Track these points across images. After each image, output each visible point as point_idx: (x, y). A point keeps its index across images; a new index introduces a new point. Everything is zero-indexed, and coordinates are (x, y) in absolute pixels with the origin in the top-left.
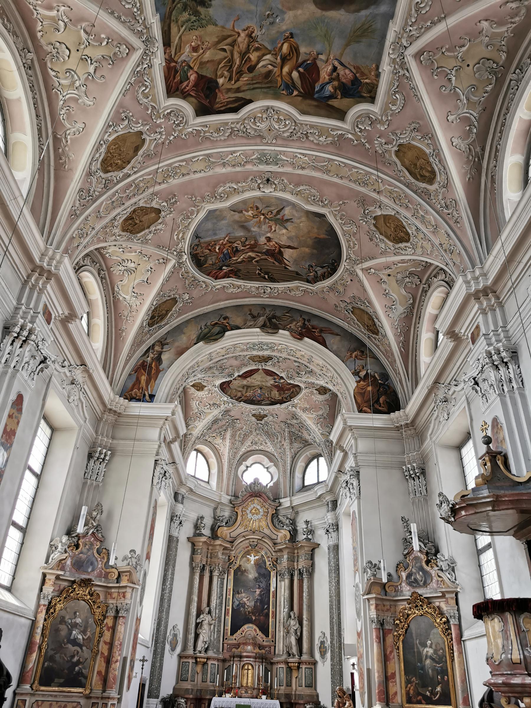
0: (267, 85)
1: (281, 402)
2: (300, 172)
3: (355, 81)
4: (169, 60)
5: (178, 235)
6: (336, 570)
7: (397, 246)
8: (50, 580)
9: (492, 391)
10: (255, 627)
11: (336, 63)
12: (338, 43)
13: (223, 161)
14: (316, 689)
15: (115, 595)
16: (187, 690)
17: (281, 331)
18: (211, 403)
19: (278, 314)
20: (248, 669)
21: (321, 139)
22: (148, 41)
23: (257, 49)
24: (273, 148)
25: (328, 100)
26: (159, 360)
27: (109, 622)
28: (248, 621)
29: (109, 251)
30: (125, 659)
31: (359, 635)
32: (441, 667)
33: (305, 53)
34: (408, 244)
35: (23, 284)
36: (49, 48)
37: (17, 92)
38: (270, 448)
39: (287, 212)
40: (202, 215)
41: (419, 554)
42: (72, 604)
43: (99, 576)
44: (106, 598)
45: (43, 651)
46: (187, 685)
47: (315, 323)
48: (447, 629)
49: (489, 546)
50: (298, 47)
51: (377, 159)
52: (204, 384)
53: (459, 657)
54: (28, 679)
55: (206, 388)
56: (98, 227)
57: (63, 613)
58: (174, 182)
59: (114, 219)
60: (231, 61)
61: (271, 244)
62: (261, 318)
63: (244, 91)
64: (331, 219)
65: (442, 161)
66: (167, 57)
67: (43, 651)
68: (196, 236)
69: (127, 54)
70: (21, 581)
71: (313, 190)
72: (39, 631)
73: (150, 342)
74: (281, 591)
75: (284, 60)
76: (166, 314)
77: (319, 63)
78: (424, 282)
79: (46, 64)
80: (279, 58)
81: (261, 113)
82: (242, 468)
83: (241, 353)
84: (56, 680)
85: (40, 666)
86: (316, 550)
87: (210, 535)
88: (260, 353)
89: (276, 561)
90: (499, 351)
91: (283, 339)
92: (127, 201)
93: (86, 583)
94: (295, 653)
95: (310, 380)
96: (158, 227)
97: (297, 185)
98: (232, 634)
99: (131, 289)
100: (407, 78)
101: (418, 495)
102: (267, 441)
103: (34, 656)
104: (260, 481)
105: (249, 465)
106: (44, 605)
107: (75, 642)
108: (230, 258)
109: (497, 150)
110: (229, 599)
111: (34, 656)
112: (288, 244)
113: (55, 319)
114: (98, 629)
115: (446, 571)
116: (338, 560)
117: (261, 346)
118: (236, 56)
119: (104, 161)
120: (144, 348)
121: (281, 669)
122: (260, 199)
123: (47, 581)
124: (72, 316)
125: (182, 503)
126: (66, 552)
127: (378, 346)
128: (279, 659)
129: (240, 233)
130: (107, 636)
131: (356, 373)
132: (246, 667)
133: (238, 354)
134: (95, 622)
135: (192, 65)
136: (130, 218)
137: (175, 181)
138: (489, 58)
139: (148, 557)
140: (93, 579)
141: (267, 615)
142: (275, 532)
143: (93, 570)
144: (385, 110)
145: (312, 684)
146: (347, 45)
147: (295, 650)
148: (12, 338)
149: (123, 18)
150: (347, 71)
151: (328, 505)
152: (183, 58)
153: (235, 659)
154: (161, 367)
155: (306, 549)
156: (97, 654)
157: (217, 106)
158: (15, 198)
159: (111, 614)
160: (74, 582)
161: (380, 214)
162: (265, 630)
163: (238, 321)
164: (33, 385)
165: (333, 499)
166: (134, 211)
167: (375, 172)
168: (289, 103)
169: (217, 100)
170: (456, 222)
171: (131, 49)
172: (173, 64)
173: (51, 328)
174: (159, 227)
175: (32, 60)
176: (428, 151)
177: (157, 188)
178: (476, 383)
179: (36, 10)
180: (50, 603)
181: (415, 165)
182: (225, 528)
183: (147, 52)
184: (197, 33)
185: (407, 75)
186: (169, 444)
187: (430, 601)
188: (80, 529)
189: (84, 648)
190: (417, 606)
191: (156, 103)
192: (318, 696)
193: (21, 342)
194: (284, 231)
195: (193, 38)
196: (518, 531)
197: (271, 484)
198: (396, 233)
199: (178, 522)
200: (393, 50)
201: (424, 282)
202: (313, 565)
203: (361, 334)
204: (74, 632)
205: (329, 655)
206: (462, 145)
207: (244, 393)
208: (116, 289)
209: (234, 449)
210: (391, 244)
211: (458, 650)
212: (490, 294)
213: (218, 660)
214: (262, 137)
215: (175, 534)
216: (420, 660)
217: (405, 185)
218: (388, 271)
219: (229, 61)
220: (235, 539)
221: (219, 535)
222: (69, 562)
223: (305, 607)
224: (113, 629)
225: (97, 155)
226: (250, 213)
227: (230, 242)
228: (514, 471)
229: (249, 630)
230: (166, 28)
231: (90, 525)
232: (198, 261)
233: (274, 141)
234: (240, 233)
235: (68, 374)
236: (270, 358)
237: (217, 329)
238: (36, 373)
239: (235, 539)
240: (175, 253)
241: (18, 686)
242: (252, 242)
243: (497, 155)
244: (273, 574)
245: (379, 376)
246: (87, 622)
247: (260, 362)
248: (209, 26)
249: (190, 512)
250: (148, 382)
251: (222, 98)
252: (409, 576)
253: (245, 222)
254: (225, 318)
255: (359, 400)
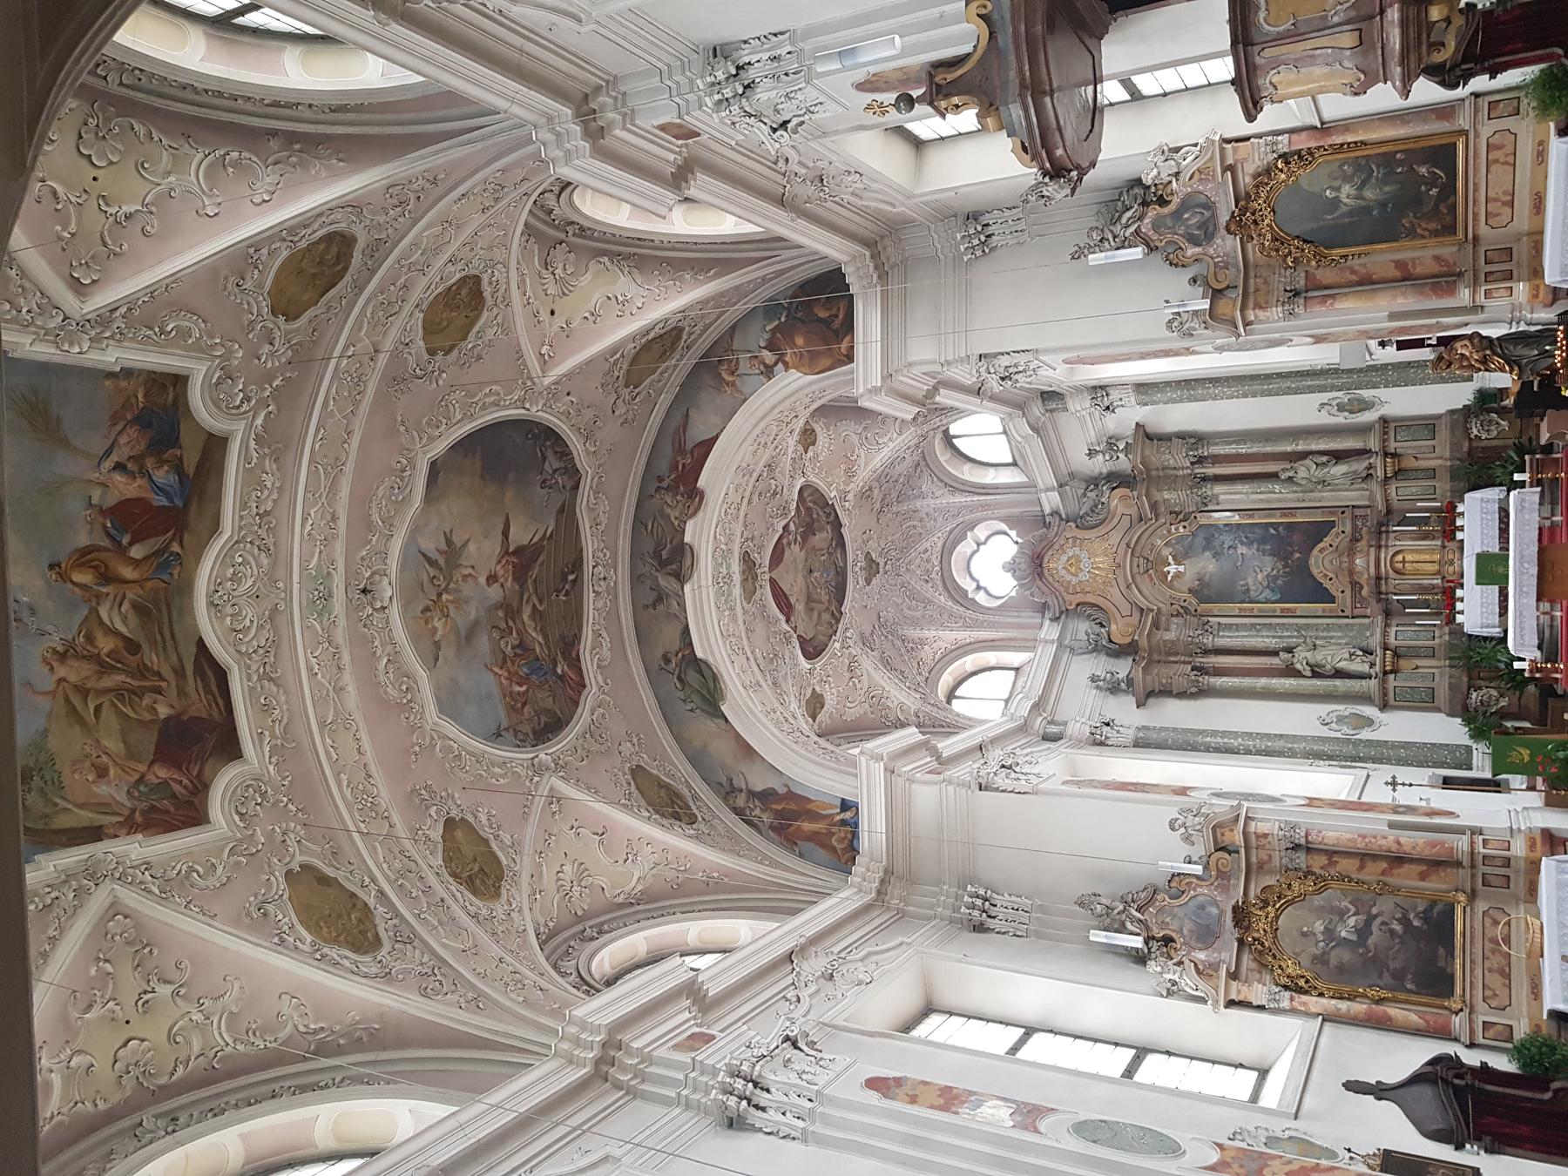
0: (164, 607)
1: (838, 525)
2: (342, 523)
3: (143, 421)
4: (131, 826)
5: (497, 777)
6: (1190, 387)
7: (489, 302)
8: (1239, 992)
9: (799, 96)
10: (1315, 552)
11: (108, 464)
12: (67, 466)
13: (332, 693)
14: (1439, 417)
15: (1263, 855)
16: (1451, 687)
17: (687, 539)
18: (847, 675)
19: (650, 546)
20: (1404, 561)
21: (269, 484)
22: (93, 873)
23: (90, 638)
24: (296, 586)
25: (187, 476)
26: (766, 796)
27: (1318, 862)
28: (1304, 567)
29: (542, 922)
30: (1392, 825)
31: (1319, 339)
32: (1378, 166)
33: (90, 533)
34: (485, 278)
35: (635, 1098)
36: (129, 1083)
37: (231, 1140)
38: (937, 541)
39: (431, 545)
40: (451, 729)
41: (1146, 221)
42: (1285, 942)
43: (1225, 889)
44: (1270, 872)
45: (1384, 994)
46: (1442, 694)
47: (663, 467)
48: (1300, 157)
49: (1127, 84)
50: (77, 550)
51: (305, 359)
52: (809, 691)
53: (1355, 132)
54: (1441, 1020)
55: (818, 689)
56: (497, 951)
57: (1305, 961)
58: (385, 795)
59: (475, 916)
60: (119, 692)
61: (501, 573)
62: (662, 582)
63: (180, 660)
64: (439, 448)
65: (305, 221)
66: (124, 831)
67: (1384, 994)
68: (496, 736)
69: (126, 917)
70: (1246, 1049)
71: (380, 493)
72: (1344, 1006)
73: (731, 819)
74: (1240, 501)
75: (107, 577)
76: (667, 786)
77: (111, 500)
78: (562, 236)
79: (161, 1087)
80: (104, 590)
81: (222, 619)
82: (981, 598)
83: (741, 622)
84: (1441, 964)
85: (1414, 998)
86: (1149, 430)
87: (1130, 659)
88: (737, 578)
89: (1178, 514)
90: (713, 84)
91: (702, 532)
92: (434, 894)
93: (1241, 916)
94: (1366, 464)
95: (789, 467)
96: (484, 821)
97: (370, 526)
98: (1332, 600)
99: (619, 868)
100: (130, 309)
101: (1022, 226)
102: (921, 549)
103: (1394, 1012)
104: (1008, 558)
105: (974, 585)
106: (1292, 999)
107: (1363, 932)
108: (537, 659)
109: (276, 104)
110: (1260, 610)
111: (1394, 1012)
112: (500, 537)
113: (700, 1026)
114: (1334, 884)
115: (1178, 164)
116: (1168, 384)
117: (722, 581)
118: (109, 681)
119: (357, 948)
120: (743, 829)
121: (1400, 492)
122: (406, 605)
123: (1241, 998)
124: (691, 991)
125: (1065, 724)
126: (1180, 963)
127: (707, 327)
128: (1379, 498)
129: (484, 642)
130: (1348, 866)
131: (769, 372)
132: (1400, 566)
133: (742, 627)
134: (1319, 892)
135: (136, 776)
136: (471, 884)
137: (383, 793)
138: (76, 137)
139: (1183, 791)
140: (1233, 902)
141: (1290, 527)
142: (1115, 521)
143: (1216, 904)
144: (202, 350)
145: (1426, 425)
146: (64, 443)
147: (1359, 466)
148: (752, 1110)
149: (51, 933)
150: (123, 440)
151: (1051, 411)
152: (122, 797)
153: (1383, 589)
154: (782, 790)
155: (1147, 452)
156: (1385, 884)
157: (215, 714)
158: (461, 1127)
159: (1301, 859)
160: (1241, 942)
161: (422, 343)
162: (1319, 531)
163: (671, 633)
164: (842, 1060)
165: (1039, 401)
166: (454, 875)
167: (333, 362)
168: (198, 558)
169: (204, 715)
170: (435, 181)
171: (115, 910)
172: (138, 817)
173: (722, 1031)
174: (483, 818)
175: (157, 1117)
176: (285, 253)
177: (401, 830)
178: (784, 125)
179: (52, 1117)
180: (1286, 987)
181: (314, 276)
182: (1114, 627)
183: (117, 875)
184: (66, 772)
185: (123, 310)
186: (943, 762)
187: (1243, 194)
188: (1137, 942)
189: (1374, 911)
190: (1255, 222)
191: (222, 849)
192: (1452, 412)
193: (758, 1091)
194: (472, 547)
195: (78, 781)
196: (1090, 31)
197: (1013, 533)
198: (460, 306)
199: (1106, 729)
200: (71, 344)
201: (562, 236)
202: (1182, 436)
203: (682, 364)
204: (1343, 934)
205: (1366, 394)
206: (268, 180)
207: (822, 607)
208: (621, 899)
209: (945, 620)
210: (485, 314)
211: (1343, 133)
212: (588, 104)
213: (1387, 625)
214: (275, 610)
215: (1129, 735)
216: (1367, 210)
217: (357, 296)
218: (544, 316)
219: (120, 697)
220: (1133, 604)
221: (1129, 640)
222: (1201, 956)
223: (1269, 449)
224: (1332, 854)
225: (346, 963)
226: (438, 624)
227: (504, 661)
228: (968, 48)
229: (1322, 563)
230: (64, 839)
231: (1123, 917)
232: (548, 728)
233: (281, 585)
234: (484, 642)
235: (812, 988)
236: (747, 559)
237: (692, 677)
238: (819, 1055)
239: (1133, 604)
240: (536, 779)
241: (1456, 1040)
242: (501, 614)
243: (283, 104)
244: (1203, 519)
245: (771, 321)
246: (1321, 909)
247: (755, 578)
248: (50, 746)
249: (1081, 702)
250: (814, 816)
251: (199, 705)
252: (1195, 242)
253: (458, 634)
254: (667, 661)
255: (827, 362)
